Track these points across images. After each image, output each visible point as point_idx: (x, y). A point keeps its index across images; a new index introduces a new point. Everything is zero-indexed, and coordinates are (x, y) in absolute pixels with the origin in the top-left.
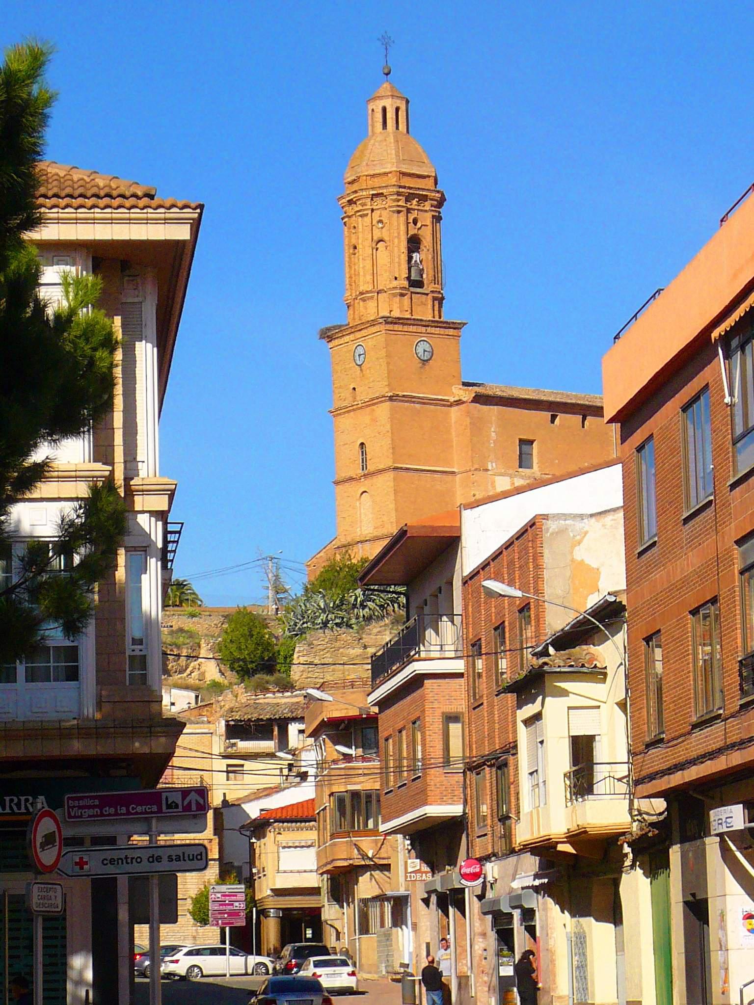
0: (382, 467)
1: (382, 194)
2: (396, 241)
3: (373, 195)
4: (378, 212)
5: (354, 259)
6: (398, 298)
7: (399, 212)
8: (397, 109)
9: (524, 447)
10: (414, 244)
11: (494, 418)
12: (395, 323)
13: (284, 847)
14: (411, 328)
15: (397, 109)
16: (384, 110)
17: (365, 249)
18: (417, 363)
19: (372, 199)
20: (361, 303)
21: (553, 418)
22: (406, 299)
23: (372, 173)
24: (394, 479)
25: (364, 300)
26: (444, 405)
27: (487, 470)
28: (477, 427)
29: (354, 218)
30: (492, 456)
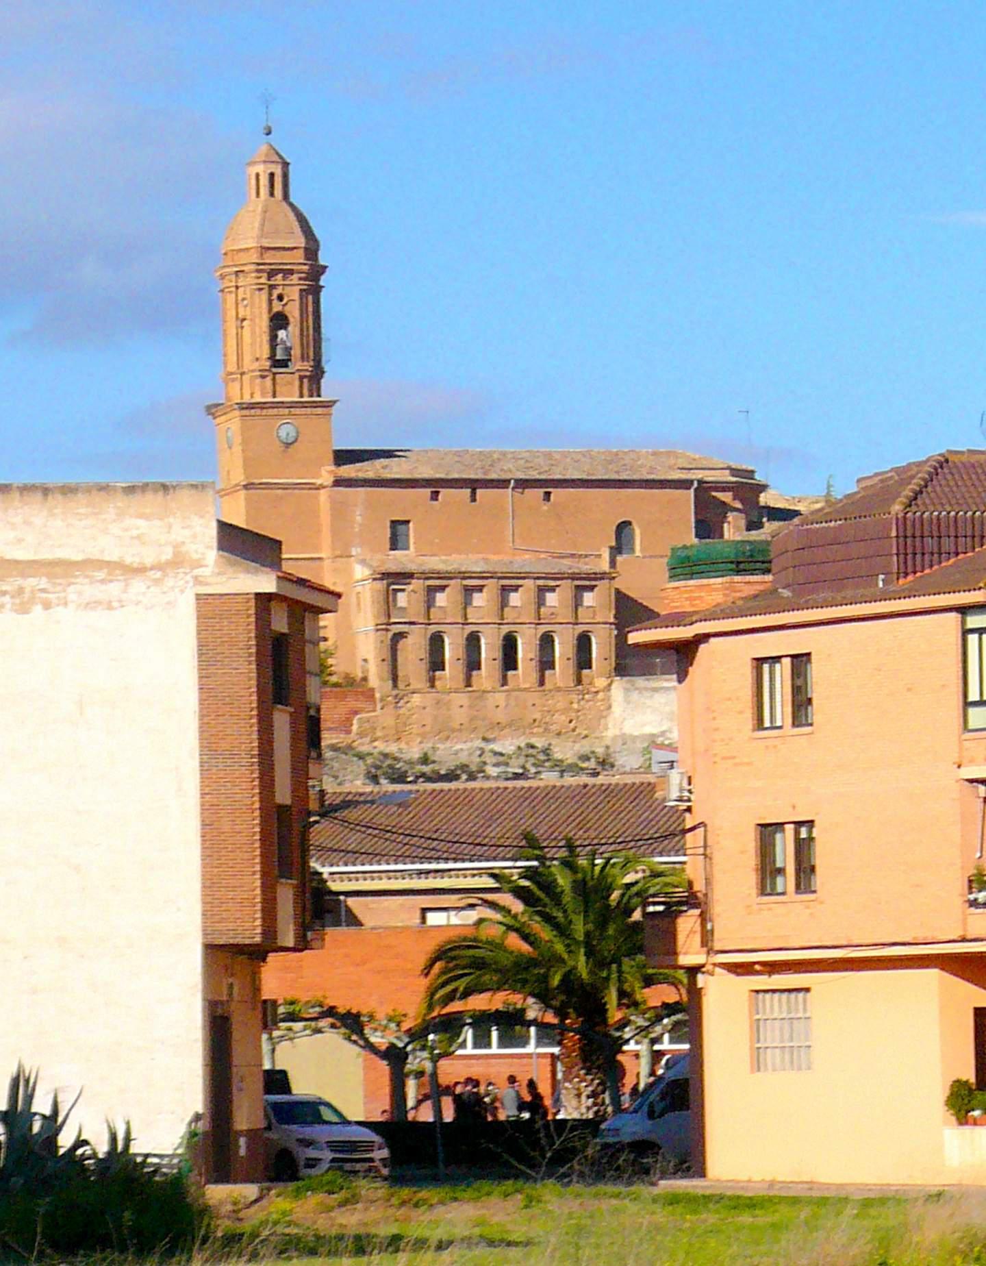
6: (258, 381)
7: (260, 289)
8: (272, 175)
10: (279, 321)
14: (271, 412)
16: (258, 175)
18: (279, 447)
28: (340, 512)
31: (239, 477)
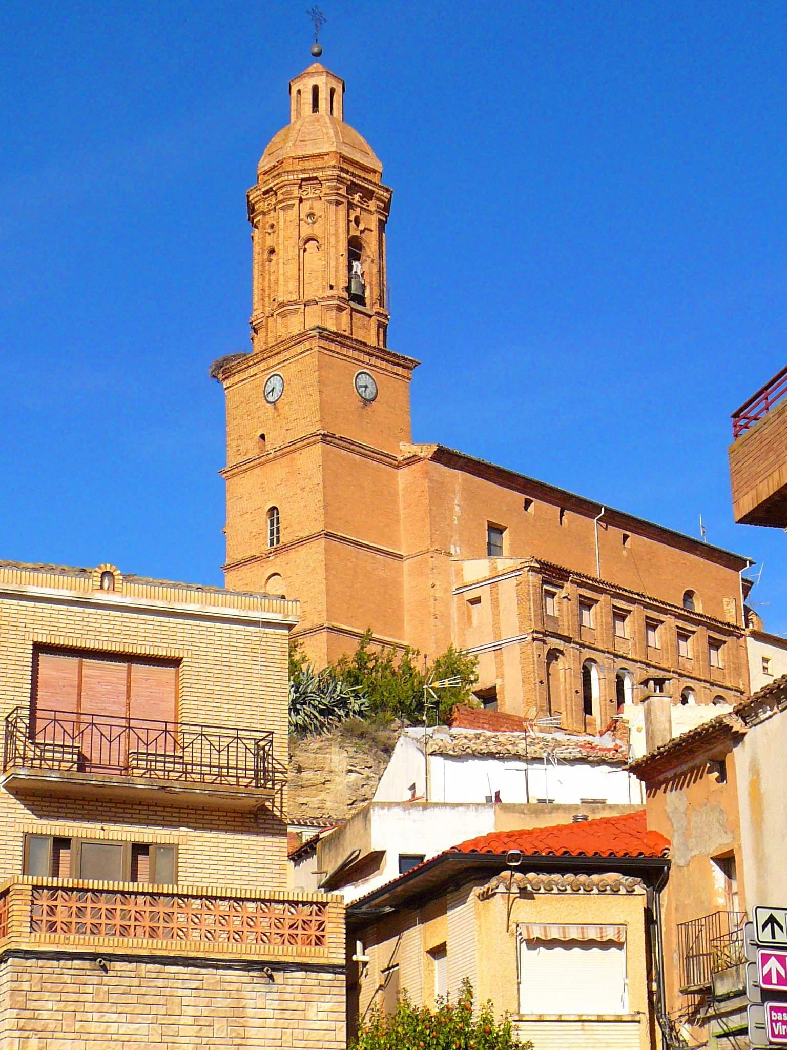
0: (304, 535)
1: (316, 178)
2: (333, 240)
3: (303, 180)
4: (309, 203)
7: (338, 203)
10: (355, 250)
11: (458, 487)
12: (332, 341)
13: (534, 943)
15: (332, 91)
16: (315, 89)
17: (287, 250)
19: (300, 187)
20: (279, 320)
21: (528, 503)
22: (345, 315)
25: (283, 315)
26: (390, 465)
27: (449, 554)
28: (438, 494)
31: (307, 422)
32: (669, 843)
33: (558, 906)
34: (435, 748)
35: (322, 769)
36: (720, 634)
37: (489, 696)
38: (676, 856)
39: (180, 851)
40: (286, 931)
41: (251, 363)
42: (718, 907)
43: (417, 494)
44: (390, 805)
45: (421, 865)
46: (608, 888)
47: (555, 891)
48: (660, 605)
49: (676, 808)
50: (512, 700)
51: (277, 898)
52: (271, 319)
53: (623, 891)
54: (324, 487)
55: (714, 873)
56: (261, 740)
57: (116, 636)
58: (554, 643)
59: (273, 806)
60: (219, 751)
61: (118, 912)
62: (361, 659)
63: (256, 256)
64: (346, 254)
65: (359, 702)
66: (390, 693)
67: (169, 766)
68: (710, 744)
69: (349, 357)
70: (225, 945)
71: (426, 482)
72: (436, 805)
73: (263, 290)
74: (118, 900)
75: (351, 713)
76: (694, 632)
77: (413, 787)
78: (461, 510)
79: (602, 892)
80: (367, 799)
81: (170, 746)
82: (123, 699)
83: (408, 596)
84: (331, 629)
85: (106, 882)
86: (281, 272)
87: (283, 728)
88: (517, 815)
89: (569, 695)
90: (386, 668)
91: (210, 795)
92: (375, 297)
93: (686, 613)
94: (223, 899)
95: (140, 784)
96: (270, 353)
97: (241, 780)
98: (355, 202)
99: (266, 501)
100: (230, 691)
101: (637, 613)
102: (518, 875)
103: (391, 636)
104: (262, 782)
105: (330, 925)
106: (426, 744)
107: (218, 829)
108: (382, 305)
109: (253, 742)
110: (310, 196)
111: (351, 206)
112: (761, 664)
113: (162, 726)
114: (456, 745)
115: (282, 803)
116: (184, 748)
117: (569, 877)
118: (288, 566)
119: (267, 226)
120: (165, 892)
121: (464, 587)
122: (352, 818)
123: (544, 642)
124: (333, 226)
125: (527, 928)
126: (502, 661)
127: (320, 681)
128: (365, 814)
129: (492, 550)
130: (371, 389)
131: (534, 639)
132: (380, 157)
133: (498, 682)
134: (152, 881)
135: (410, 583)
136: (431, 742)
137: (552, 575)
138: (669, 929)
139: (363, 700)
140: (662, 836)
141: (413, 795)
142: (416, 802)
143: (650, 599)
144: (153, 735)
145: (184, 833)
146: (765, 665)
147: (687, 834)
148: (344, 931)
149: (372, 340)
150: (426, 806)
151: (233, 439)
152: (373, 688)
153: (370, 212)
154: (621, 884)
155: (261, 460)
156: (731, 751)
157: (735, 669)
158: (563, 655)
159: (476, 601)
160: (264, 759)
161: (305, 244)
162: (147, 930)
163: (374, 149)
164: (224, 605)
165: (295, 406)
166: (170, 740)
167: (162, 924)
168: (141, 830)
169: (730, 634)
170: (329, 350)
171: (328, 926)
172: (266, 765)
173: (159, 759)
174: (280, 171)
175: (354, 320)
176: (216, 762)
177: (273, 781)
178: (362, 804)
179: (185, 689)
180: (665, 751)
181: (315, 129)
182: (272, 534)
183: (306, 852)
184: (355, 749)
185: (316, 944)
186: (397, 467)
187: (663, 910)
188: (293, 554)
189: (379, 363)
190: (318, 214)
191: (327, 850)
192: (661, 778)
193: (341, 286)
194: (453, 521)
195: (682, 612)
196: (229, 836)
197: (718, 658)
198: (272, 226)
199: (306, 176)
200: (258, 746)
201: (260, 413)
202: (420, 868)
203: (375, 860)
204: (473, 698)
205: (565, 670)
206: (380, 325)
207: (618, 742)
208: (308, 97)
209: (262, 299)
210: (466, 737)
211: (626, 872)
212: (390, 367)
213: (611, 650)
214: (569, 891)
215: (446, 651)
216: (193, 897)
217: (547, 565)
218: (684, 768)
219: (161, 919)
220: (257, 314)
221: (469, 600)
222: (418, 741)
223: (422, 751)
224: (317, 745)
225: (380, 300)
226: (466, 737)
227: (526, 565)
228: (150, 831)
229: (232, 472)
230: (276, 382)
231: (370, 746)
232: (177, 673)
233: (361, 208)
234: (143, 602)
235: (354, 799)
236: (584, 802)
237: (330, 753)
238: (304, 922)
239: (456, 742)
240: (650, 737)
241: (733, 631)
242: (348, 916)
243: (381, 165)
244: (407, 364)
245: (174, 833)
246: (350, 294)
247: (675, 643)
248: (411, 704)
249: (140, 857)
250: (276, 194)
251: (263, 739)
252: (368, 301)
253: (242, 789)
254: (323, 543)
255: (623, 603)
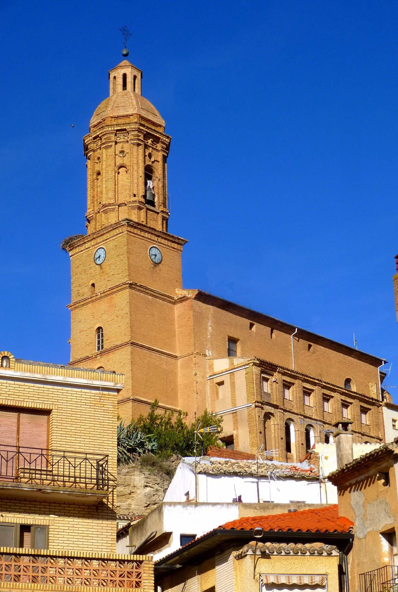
0: (118, 343)
1: (125, 130)
3: (117, 130)
5: (99, 183)
7: (139, 145)
9: (231, 344)
10: (149, 173)
11: (210, 316)
12: (135, 228)
15: (135, 77)
16: (125, 76)
17: (108, 172)
19: (116, 135)
20: (103, 215)
21: (251, 325)
22: (143, 213)
23: (116, 115)
24: (132, 353)
25: (105, 212)
26: (170, 302)
27: (205, 356)
29: (99, 151)
30: (209, 345)
32: (353, 524)
33: (285, 563)
34: (201, 469)
35: (129, 485)
36: (367, 404)
37: (229, 441)
38: (358, 532)
39: (50, 530)
40: (118, 579)
41: (87, 240)
42: (384, 563)
43: (186, 320)
44: (175, 504)
45: (193, 541)
46: (316, 552)
47: (283, 553)
48: (331, 387)
49: (357, 503)
50: (244, 441)
51: (111, 558)
52: (98, 214)
53: (325, 554)
54: (131, 315)
55: (382, 542)
56: (100, 460)
57: (10, 396)
58: (268, 409)
59: (108, 501)
60: (75, 467)
61: (13, 566)
62: (153, 418)
63: (89, 176)
64: (143, 176)
65: (151, 444)
66: (170, 439)
67: (44, 477)
68: (379, 462)
69: (145, 238)
70: (80, 587)
71: (191, 313)
72: (203, 504)
73: (94, 197)
74: (13, 559)
75: (147, 451)
76: (351, 403)
77: (187, 494)
78: (212, 329)
79: (312, 554)
80: (156, 503)
81: (44, 464)
82: (15, 435)
83: (180, 380)
84: (135, 400)
85: (5, 548)
86: (104, 186)
87: (114, 453)
88: (252, 510)
89: (277, 440)
90: (167, 423)
91: (69, 495)
92: (161, 202)
93: (347, 392)
94: (78, 558)
95: (26, 488)
96: (98, 234)
97: (88, 485)
98: (148, 144)
99: (95, 324)
100: (83, 427)
101: (318, 391)
102: (260, 544)
103: (170, 404)
104: (101, 486)
105: (145, 575)
106: (196, 467)
107: (74, 516)
108: (165, 206)
109: (95, 462)
110: (122, 140)
111: (146, 147)
112: (391, 423)
113: (39, 452)
114: (214, 468)
115: (113, 499)
116: (53, 465)
117: (292, 545)
118: (108, 363)
119: (96, 158)
120: (42, 554)
121: (214, 375)
122: (149, 514)
123: (262, 408)
124: (136, 158)
125: (266, 577)
126: (237, 420)
127: (128, 432)
128: (160, 510)
129: (231, 353)
130: (159, 256)
131: (256, 407)
132: (164, 117)
133: (235, 433)
134: (33, 547)
135: (182, 374)
136: (199, 466)
137: (267, 368)
138: (353, 578)
139: (154, 443)
140: (348, 520)
141: (188, 499)
142: (190, 502)
143: (325, 383)
144: (34, 457)
145: (53, 519)
146: (394, 423)
147: (364, 518)
148: (153, 578)
149: (159, 226)
150: (197, 504)
151: (75, 287)
152: (160, 435)
153: (158, 151)
154: (324, 549)
155: (92, 299)
156: (393, 466)
157: (376, 425)
158: (273, 416)
159: (221, 383)
160: (102, 473)
161: (119, 169)
162: (31, 577)
163: (161, 114)
164: (78, 377)
165: (113, 267)
166: (44, 460)
167: (40, 574)
168: (26, 517)
169: (373, 404)
170: (134, 233)
171: (144, 575)
172: (104, 476)
173: (37, 472)
174: (103, 125)
175: (148, 215)
176: (73, 473)
177: (108, 485)
178: (153, 506)
179: (53, 429)
180: (351, 467)
181: (124, 99)
182: (99, 343)
183: (122, 534)
184: (149, 473)
185: (136, 587)
186: (174, 303)
187: (349, 566)
188: (111, 356)
189: (163, 241)
190: (126, 151)
191: (136, 532)
192: (347, 484)
193: (141, 195)
194: (207, 335)
195: (344, 391)
196: (80, 520)
197: (366, 419)
198: (99, 158)
199: (119, 128)
200: (99, 464)
201: (91, 271)
202: (192, 543)
203: (165, 538)
204: (219, 442)
205: (275, 425)
206: (164, 219)
207: (312, 466)
208: (120, 81)
209: (93, 202)
210: (219, 463)
211: (326, 541)
212: (170, 243)
213: (303, 413)
214: (292, 553)
215: (203, 413)
216: (59, 557)
217: (264, 362)
218: (362, 477)
219: (40, 571)
220: (90, 212)
221: (218, 383)
222: (191, 465)
223: (193, 472)
224: (126, 471)
225: (164, 204)
226: (219, 463)
227: (251, 362)
228: (32, 517)
229: (75, 306)
230: (101, 252)
231: (158, 471)
232: (48, 419)
233: (153, 148)
234: (27, 375)
235: (148, 503)
236: (291, 502)
237: (134, 475)
238: (128, 572)
239: (213, 466)
240: (340, 458)
241: (374, 403)
242: (155, 570)
243: (164, 122)
244: (180, 242)
245: (46, 518)
246: (146, 200)
247: (340, 410)
248: (182, 446)
249: (26, 534)
250: (101, 139)
251: (102, 459)
252: (156, 204)
253: (89, 491)
254: (130, 349)
255: (309, 383)
